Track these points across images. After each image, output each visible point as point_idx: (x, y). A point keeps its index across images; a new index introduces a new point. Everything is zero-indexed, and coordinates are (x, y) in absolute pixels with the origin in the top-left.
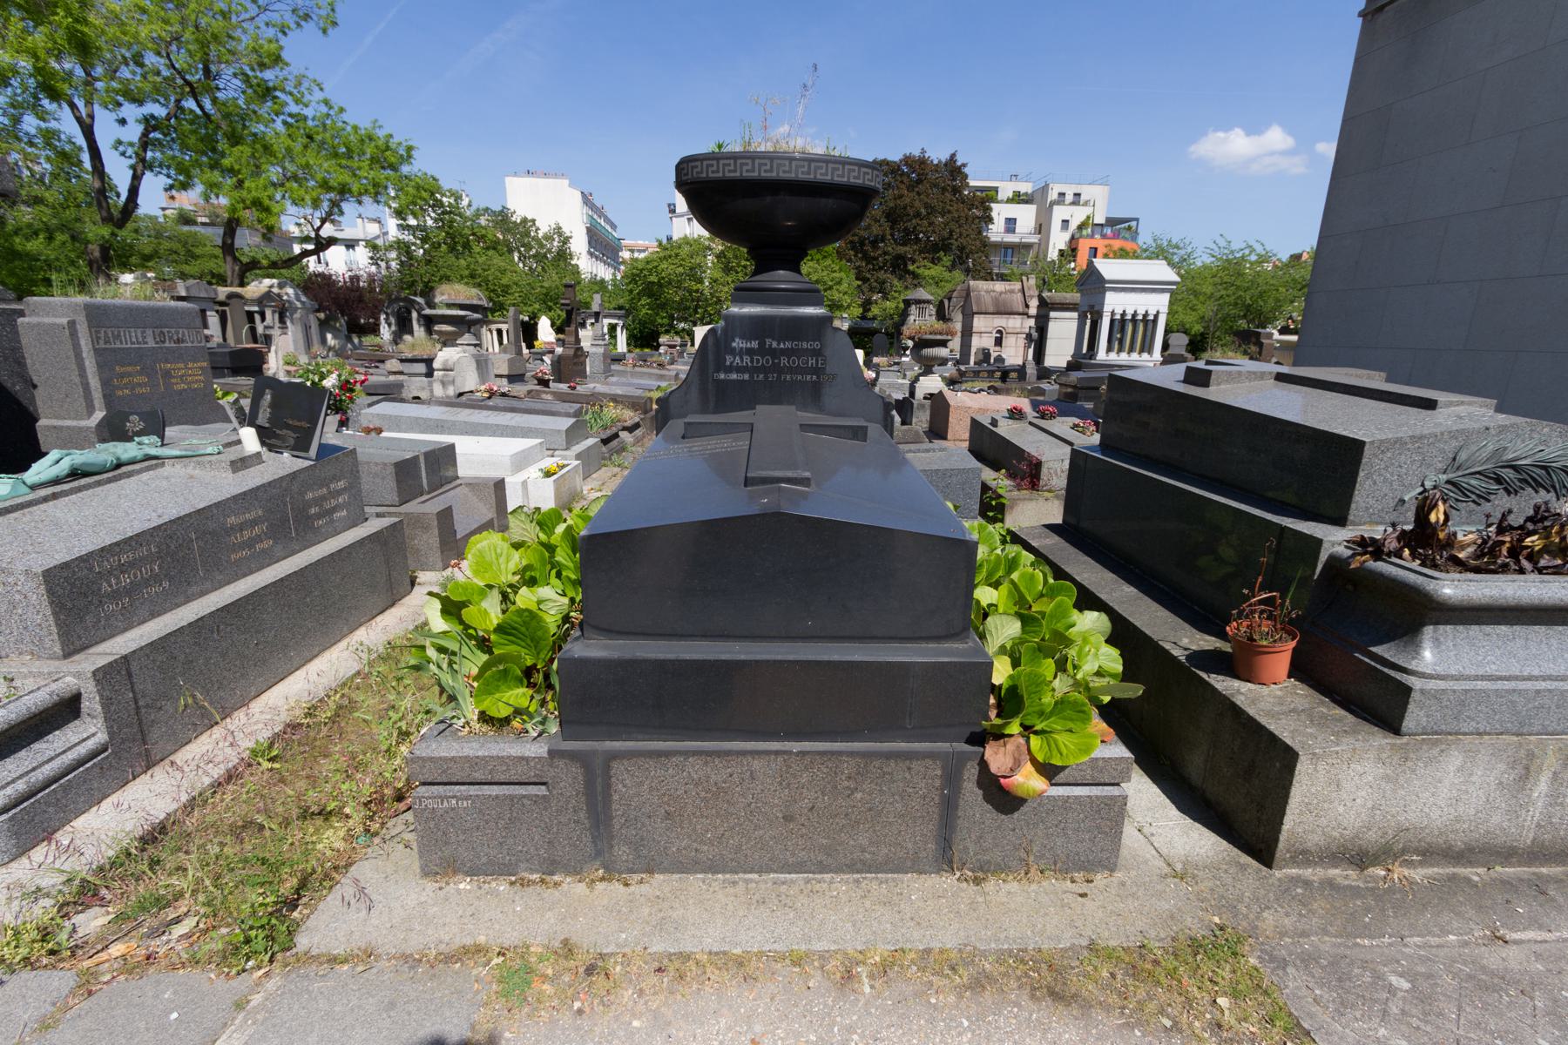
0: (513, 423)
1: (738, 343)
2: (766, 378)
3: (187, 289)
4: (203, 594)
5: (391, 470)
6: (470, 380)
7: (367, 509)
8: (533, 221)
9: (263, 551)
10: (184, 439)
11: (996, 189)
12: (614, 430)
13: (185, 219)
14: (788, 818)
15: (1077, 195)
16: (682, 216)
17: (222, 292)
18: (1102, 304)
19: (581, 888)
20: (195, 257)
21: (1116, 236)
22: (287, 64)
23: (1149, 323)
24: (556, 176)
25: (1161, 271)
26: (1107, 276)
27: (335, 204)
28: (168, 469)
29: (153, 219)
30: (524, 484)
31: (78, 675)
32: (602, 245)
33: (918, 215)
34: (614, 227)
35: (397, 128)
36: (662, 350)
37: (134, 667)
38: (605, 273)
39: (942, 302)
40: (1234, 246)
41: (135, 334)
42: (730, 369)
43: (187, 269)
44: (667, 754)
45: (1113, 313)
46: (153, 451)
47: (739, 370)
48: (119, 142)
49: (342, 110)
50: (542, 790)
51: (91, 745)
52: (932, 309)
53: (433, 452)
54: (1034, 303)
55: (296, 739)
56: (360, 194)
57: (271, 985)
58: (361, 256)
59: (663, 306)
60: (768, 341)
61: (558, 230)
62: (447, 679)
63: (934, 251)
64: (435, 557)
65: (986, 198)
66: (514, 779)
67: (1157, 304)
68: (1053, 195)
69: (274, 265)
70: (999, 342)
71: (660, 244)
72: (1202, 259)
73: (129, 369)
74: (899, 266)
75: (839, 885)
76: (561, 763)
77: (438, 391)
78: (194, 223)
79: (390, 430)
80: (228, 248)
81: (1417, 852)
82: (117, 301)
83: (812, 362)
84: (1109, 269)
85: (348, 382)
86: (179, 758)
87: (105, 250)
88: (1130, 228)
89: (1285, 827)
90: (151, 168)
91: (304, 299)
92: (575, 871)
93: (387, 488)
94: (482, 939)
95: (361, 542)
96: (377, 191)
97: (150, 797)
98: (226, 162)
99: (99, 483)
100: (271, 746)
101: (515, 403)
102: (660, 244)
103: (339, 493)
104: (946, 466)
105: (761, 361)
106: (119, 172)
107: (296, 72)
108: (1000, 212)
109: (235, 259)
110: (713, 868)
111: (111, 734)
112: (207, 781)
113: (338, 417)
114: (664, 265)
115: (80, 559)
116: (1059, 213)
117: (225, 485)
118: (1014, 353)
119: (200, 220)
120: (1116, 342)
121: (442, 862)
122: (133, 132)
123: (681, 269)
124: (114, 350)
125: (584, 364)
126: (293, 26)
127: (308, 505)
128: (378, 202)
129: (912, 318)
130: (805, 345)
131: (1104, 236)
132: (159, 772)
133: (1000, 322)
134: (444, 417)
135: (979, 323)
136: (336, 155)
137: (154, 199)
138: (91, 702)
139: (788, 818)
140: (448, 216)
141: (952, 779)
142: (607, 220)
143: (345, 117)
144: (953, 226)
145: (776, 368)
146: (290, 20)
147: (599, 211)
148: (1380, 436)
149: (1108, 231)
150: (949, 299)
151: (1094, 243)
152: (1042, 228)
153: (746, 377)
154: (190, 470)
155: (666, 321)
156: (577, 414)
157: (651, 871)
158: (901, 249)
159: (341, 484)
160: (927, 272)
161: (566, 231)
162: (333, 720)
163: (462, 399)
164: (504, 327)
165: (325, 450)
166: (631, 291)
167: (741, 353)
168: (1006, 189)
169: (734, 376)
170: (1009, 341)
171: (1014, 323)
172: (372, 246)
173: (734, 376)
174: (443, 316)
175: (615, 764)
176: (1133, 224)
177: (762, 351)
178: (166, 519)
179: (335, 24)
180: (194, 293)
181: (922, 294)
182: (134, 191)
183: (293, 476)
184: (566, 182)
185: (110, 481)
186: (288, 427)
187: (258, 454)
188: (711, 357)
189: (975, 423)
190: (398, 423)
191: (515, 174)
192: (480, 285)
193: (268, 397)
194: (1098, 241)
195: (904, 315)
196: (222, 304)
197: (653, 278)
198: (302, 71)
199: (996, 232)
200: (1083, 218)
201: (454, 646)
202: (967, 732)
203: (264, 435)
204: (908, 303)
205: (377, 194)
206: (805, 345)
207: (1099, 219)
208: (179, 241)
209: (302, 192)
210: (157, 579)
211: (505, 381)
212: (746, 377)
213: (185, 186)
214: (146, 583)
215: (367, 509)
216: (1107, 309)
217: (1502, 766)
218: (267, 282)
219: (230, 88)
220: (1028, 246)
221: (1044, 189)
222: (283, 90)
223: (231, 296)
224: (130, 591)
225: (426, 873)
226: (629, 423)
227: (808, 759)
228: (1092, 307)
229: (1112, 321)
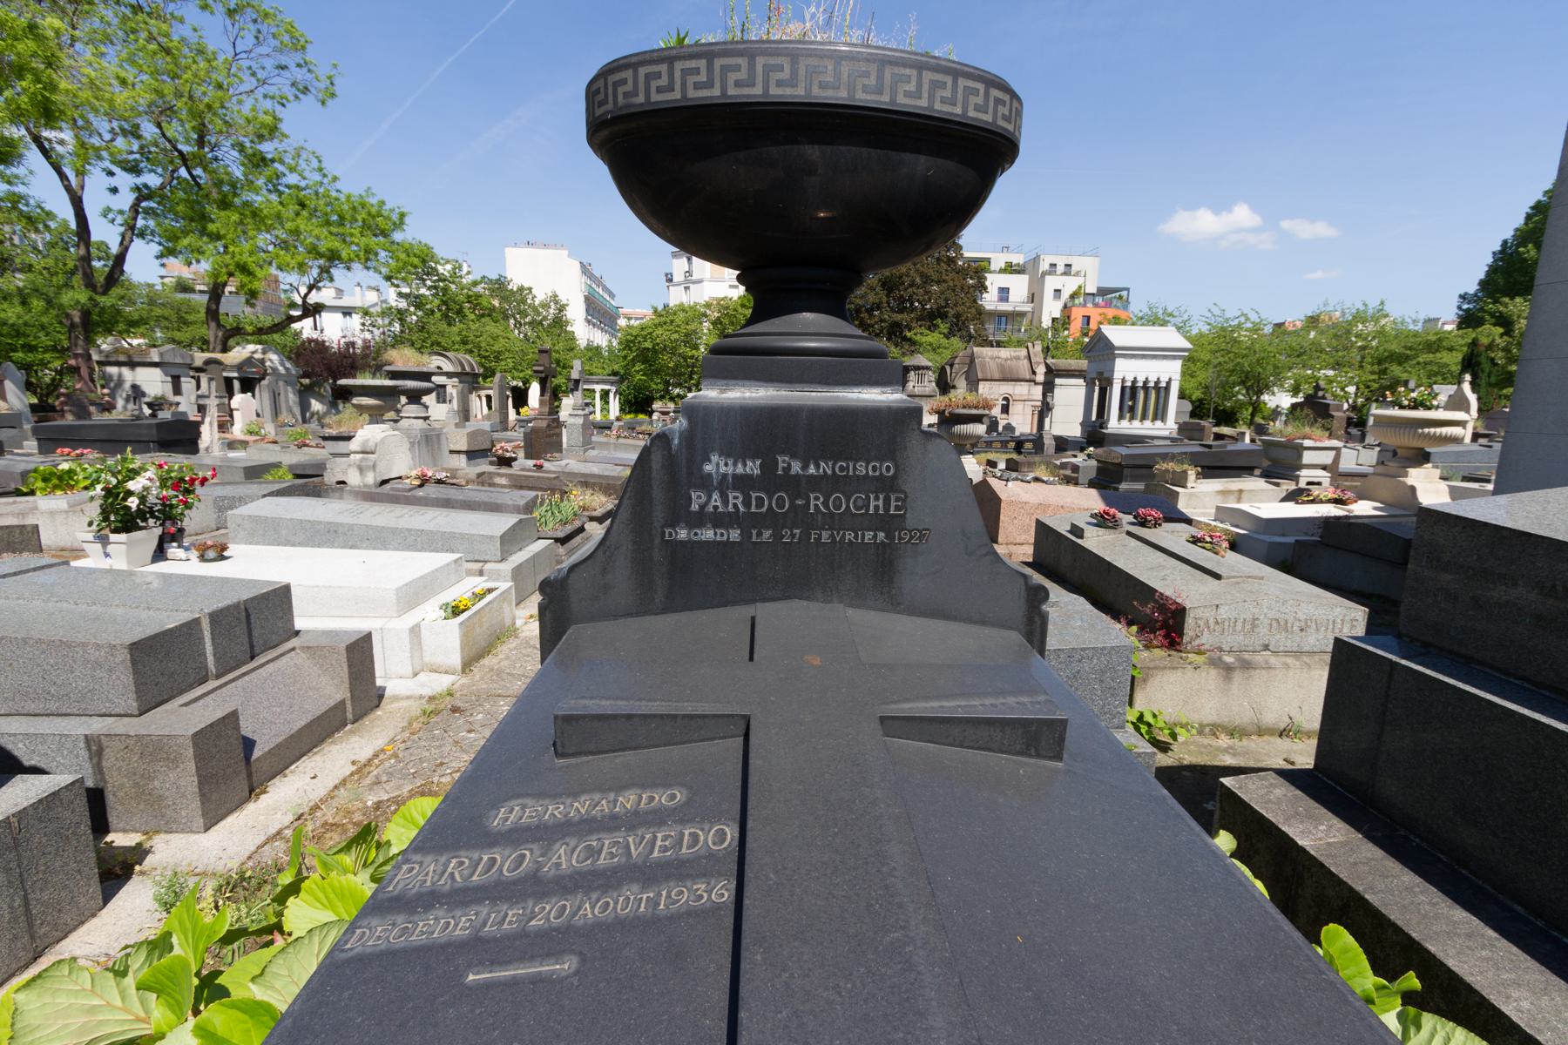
0: (431, 527)
1: (716, 465)
2: (777, 536)
3: (161, 355)
5: (123, 656)
6: (401, 463)
11: (988, 260)
12: (578, 524)
13: (183, 287)
15: (1068, 266)
16: (678, 284)
17: (200, 358)
20: (187, 323)
21: (1108, 304)
22: (286, 137)
23: (1162, 391)
24: (555, 247)
25: (1170, 337)
26: (1116, 343)
27: (325, 271)
30: (415, 631)
32: (599, 313)
33: (912, 284)
34: (612, 295)
35: (393, 198)
36: (655, 416)
38: (601, 339)
39: (943, 370)
40: (1228, 315)
42: (699, 520)
43: (178, 335)
45: (1123, 380)
47: (719, 520)
48: (109, 210)
49: (335, 179)
52: (931, 376)
54: (1041, 370)
56: (351, 260)
59: (657, 372)
60: (782, 461)
63: (930, 319)
64: (192, 807)
65: (979, 270)
67: (1170, 371)
68: (1044, 266)
69: (260, 331)
71: (655, 311)
72: (1199, 327)
78: (192, 291)
80: (213, 314)
83: (876, 503)
84: (1117, 335)
87: (86, 314)
88: (1120, 297)
90: (142, 235)
91: (288, 365)
96: (367, 257)
98: (211, 227)
102: (655, 311)
105: (763, 502)
106: (106, 233)
107: (296, 145)
108: (994, 282)
109: (219, 325)
114: (659, 331)
116: (1051, 283)
118: (1022, 422)
119: (198, 288)
120: (1127, 411)
122: (126, 200)
123: (676, 336)
125: (560, 435)
126: (291, 98)
128: (368, 268)
130: (861, 468)
131: (1096, 305)
136: (328, 223)
137: (146, 267)
142: (606, 289)
143: (338, 185)
144: (949, 294)
145: (800, 517)
146: (289, 92)
147: (598, 281)
149: (1099, 300)
150: (951, 366)
153: (735, 535)
155: (661, 387)
156: (529, 507)
158: (898, 317)
160: (924, 339)
161: (563, 298)
163: (385, 491)
166: (625, 357)
167: (724, 485)
168: (998, 261)
169: (708, 534)
170: (1015, 408)
171: (1020, 390)
173: (708, 534)
174: (363, 387)
176: (1124, 293)
177: (770, 480)
179: (333, 95)
180: (167, 359)
181: (920, 360)
184: (566, 252)
188: (658, 493)
189: (1041, 528)
191: (516, 245)
192: (471, 352)
196: (199, 370)
197: (648, 345)
198: (301, 143)
205: (367, 259)
206: (861, 468)
207: (1091, 289)
208: (172, 308)
209: (288, 258)
211: (463, 458)
212: (735, 535)
216: (1118, 376)
218: (251, 347)
220: (1022, 314)
221: (1036, 260)
222: (282, 162)
223: (208, 362)
226: (598, 513)
228: (1101, 373)
229: (1123, 389)
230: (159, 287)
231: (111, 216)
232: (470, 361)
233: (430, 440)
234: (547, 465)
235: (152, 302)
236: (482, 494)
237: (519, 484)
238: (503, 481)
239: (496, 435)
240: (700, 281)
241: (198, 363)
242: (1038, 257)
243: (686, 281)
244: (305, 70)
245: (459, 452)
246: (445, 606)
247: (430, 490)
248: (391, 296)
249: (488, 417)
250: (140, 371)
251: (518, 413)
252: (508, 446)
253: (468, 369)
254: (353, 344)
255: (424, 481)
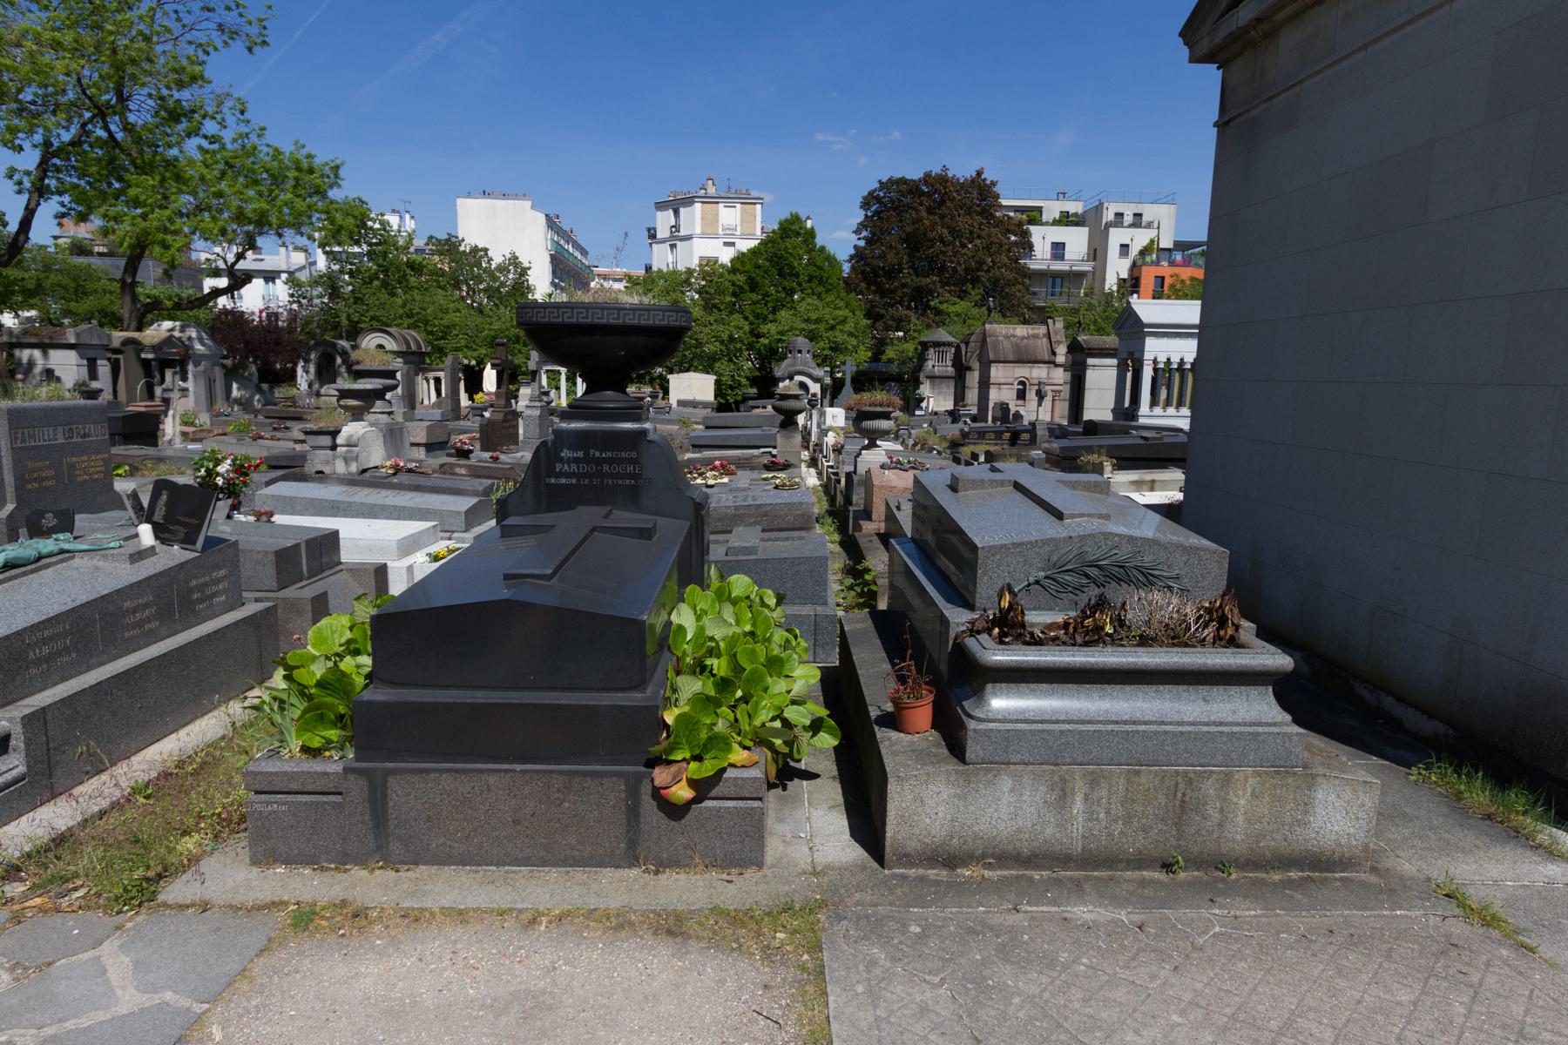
0: (411, 504)
1: (566, 453)
3: (78, 335)
4: (100, 665)
5: (272, 557)
6: (376, 455)
7: (245, 594)
8: (486, 250)
9: (151, 630)
10: (94, 531)
13: (79, 249)
14: (516, 822)
16: (663, 241)
17: (118, 336)
18: (1142, 351)
19: (364, 873)
20: (85, 293)
24: (516, 197)
26: (1145, 319)
28: (77, 562)
29: (43, 248)
31: (10, 720)
34: (584, 252)
37: (49, 718)
41: (47, 432)
42: (559, 475)
44: (427, 771)
45: (1155, 361)
46: (67, 546)
47: (568, 475)
50: (338, 799)
51: (14, 773)
53: (315, 539)
54: (1062, 350)
55: (168, 781)
57: (139, 919)
58: (281, 292)
61: (514, 260)
62: (278, 718)
63: (963, 281)
66: (319, 789)
68: (1109, 216)
70: (1021, 395)
73: (40, 464)
74: (920, 299)
75: (554, 873)
76: (352, 777)
77: (340, 468)
78: (89, 253)
79: (283, 512)
80: (128, 286)
81: (993, 856)
82: (36, 404)
83: (630, 469)
85: (242, 466)
86: (76, 791)
89: (888, 835)
92: (362, 862)
93: (268, 575)
94: (286, 898)
95: (236, 624)
97: (56, 816)
99: (25, 574)
100: (147, 786)
101: (421, 480)
103: (219, 580)
104: (796, 554)
108: (1042, 238)
109: (135, 298)
110: (463, 862)
111: (29, 767)
112: (96, 809)
113: (230, 501)
115: (18, 633)
116: (1116, 237)
117: (123, 574)
118: (1041, 413)
119: (96, 249)
121: (264, 857)
124: (28, 448)
126: (220, 45)
127: (191, 591)
129: (930, 363)
131: (1172, 263)
132: (62, 802)
133: (1022, 371)
134: (340, 498)
135: (996, 372)
138: (17, 742)
139: (516, 822)
140: (384, 245)
141: (633, 793)
147: (566, 235)
148: (997, 540)
149: (1178, 257)
150: (967, 344)
151: (1159, 271)
152: (1097, 253)
154: (95, 562)
157: (416, 863)
159: (222, 572)
160: (952, 309)
162: (195, 773)
163: (366, 478)
164: (441, 374)
165: (212, 542)
167: (569, 461)
168: (1052, 209)
169: (563, 481)
172: (292, 281)
173: (563, 481)
175: (390, 779)
177: (587, 459)
178: (78, 603)
180: (85, 340)
181: (942, 335)
182: (26, 224)
183: (181, 566)
184: (528, 204)
185: (32, 572)
186: (180, 523)
187: (153, 547)
190: (292, 506)
191: (469, 195)
193: (164, 497)
194: (1165, 269)
195: (922, 359)
196: (115, 351)
199: (1041, 257)
200: (1145, 242)
201: (284, 697)
202: (645, 757)
203: (159, 531)
204: (925, 346)
207: (1166, 243)
210: (66, 651)
211: (422, 450)
213: (83, 218)
214: (60, 653)
215: (245, 594)
216: (1148, 356)
217: (1043, 788)
218: (167, 324)
219: (141, 111)
220: (1080, 275)
221: (1098, 209)
223: (128, 342)
224: (48, 660)
225: (255, 862)
227: (528, 777)
228: (1131, 354)
229: (1155, 370)
230: (52, 250)
231: (16, 177)
232: (417, 337)
233: (393, 436)
234: (502, 457)
235: (47, 268)
236: (446, 482)
237: (476, 473)
238: (463, 471)
239: (452, 425)
240: (689, 238)
241: (116, 344)
242: (1101, 204)
243: (672, 237)
244: (234, 14)
245: (418, 445)
246: (429, 555)
247: (401, 477)
248: (322, 263)
249: (437, 405)
250: (53, 353)
251: (471, 398)
252: (464, 437)
253: (414, 348)
254: (276, 315)
255: (397, 470)
